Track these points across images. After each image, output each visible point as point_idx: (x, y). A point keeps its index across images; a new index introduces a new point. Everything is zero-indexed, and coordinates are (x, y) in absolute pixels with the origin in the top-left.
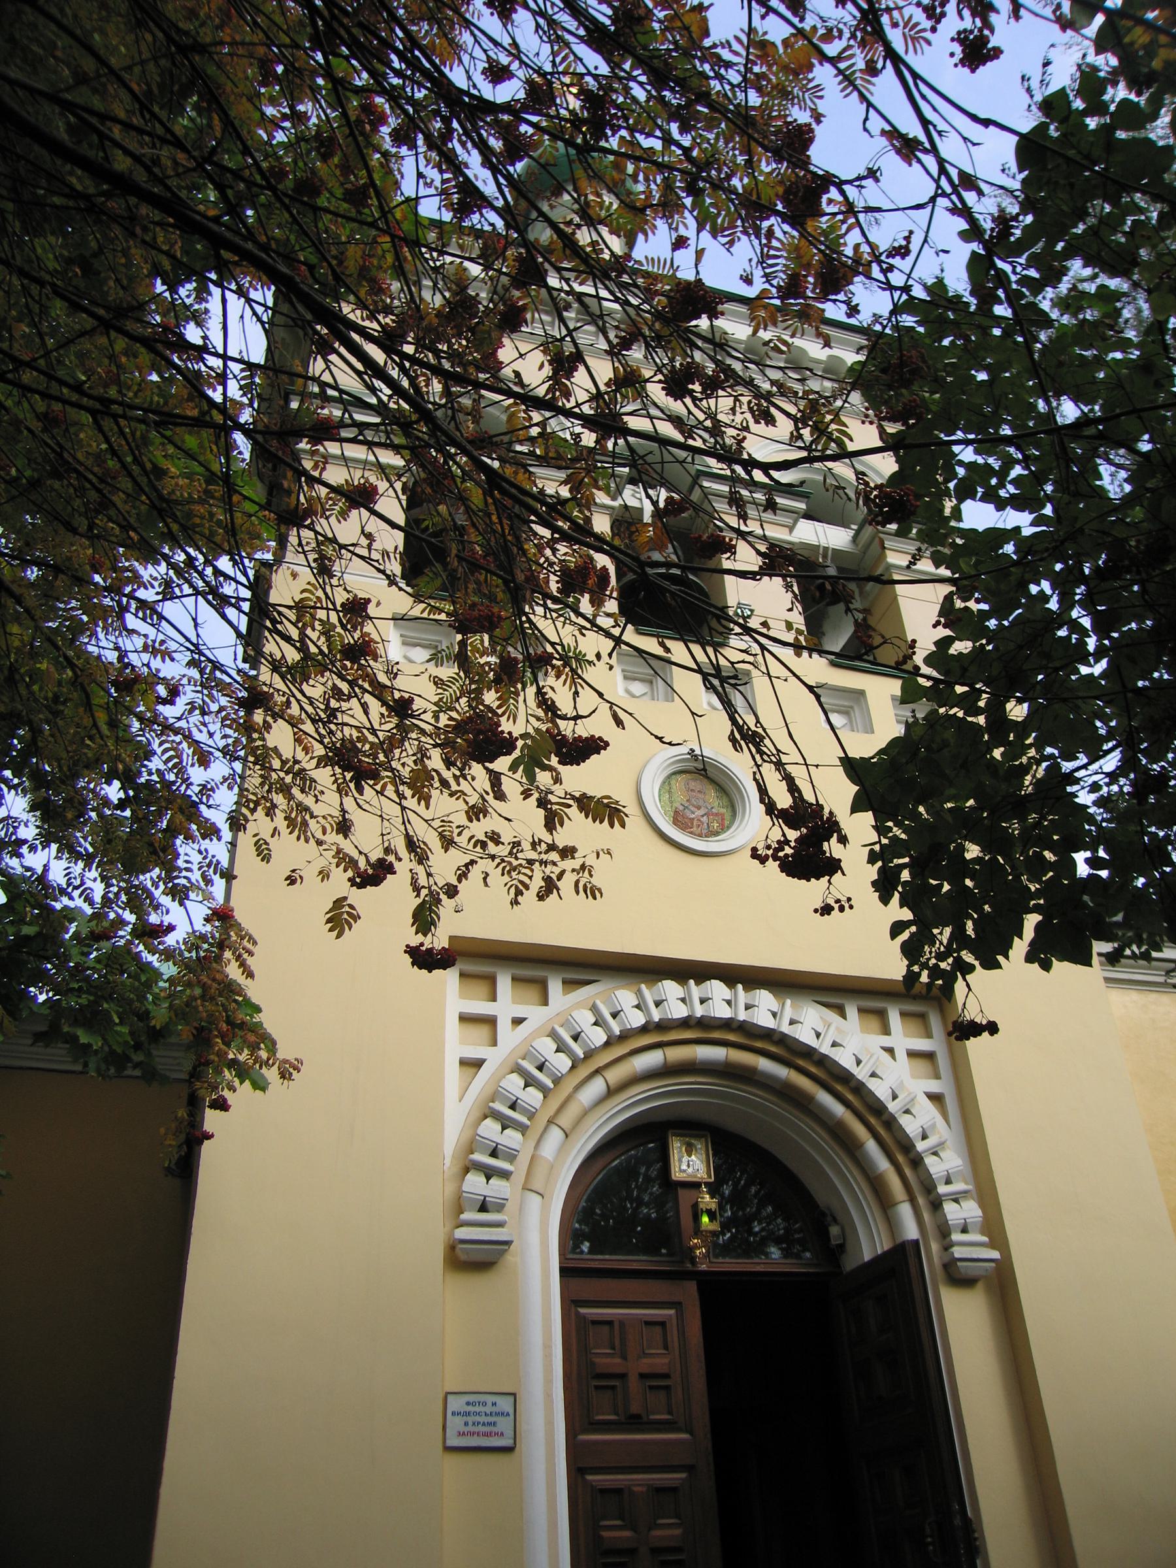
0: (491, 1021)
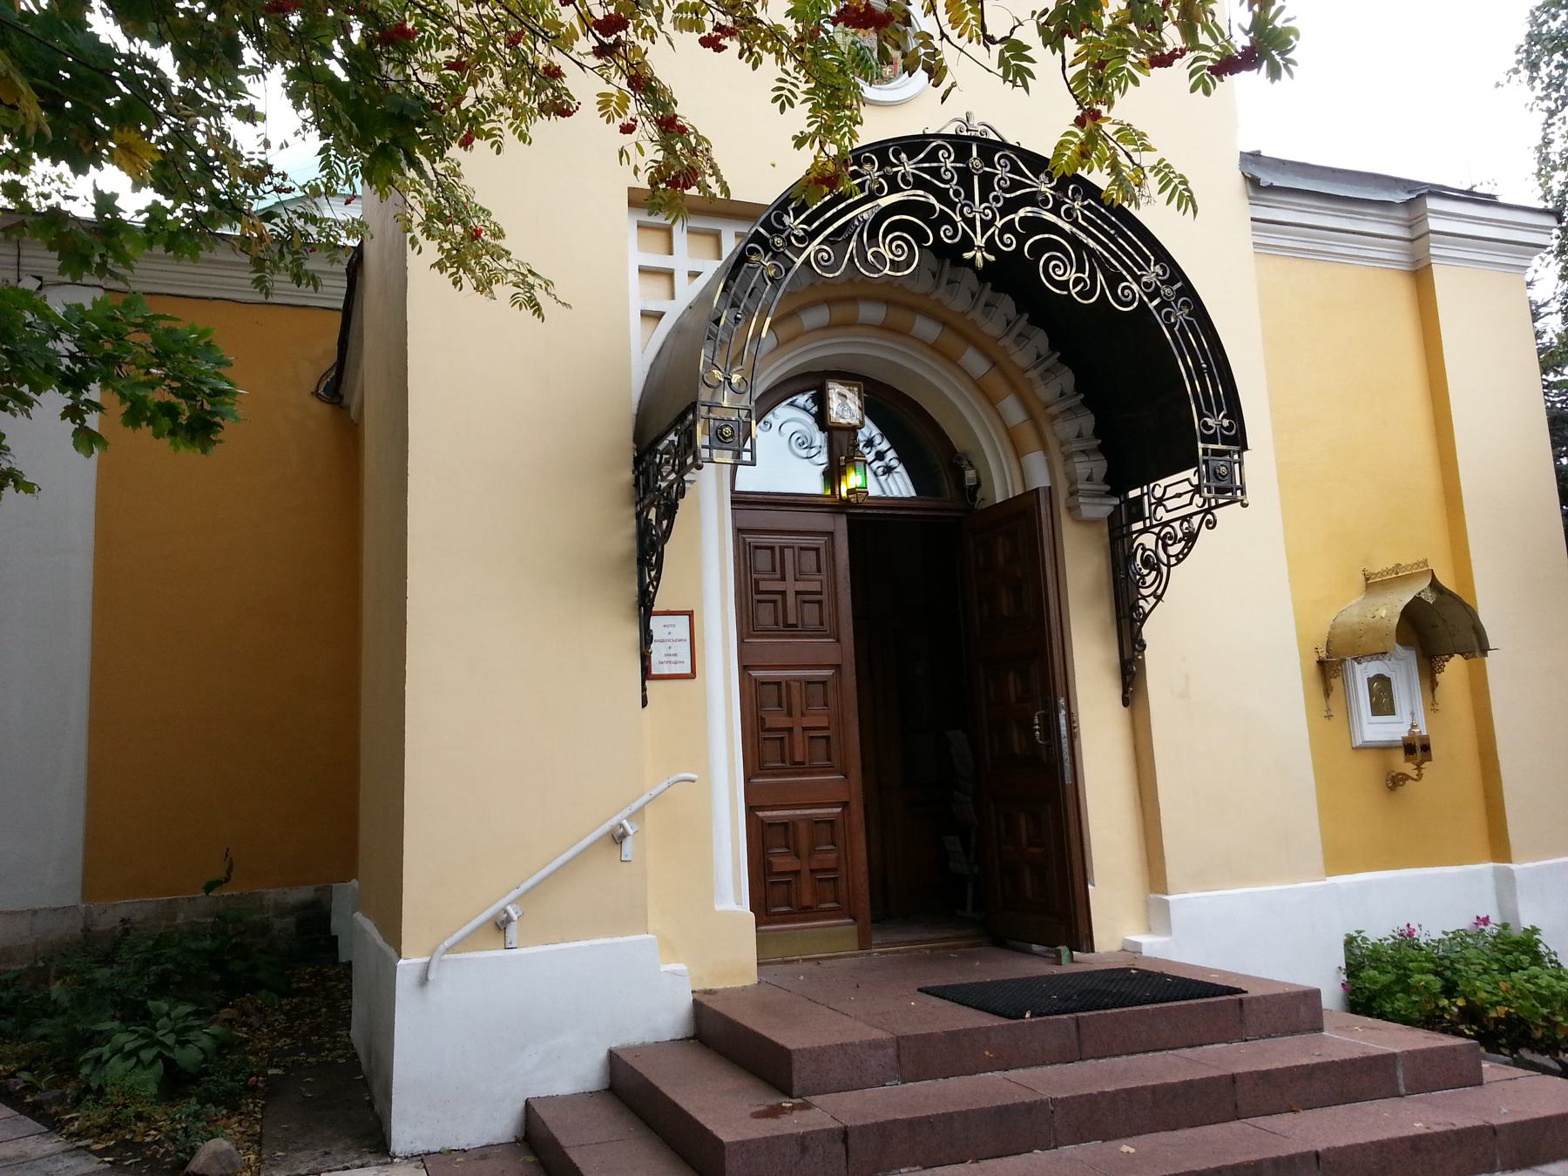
0: (669, 274)
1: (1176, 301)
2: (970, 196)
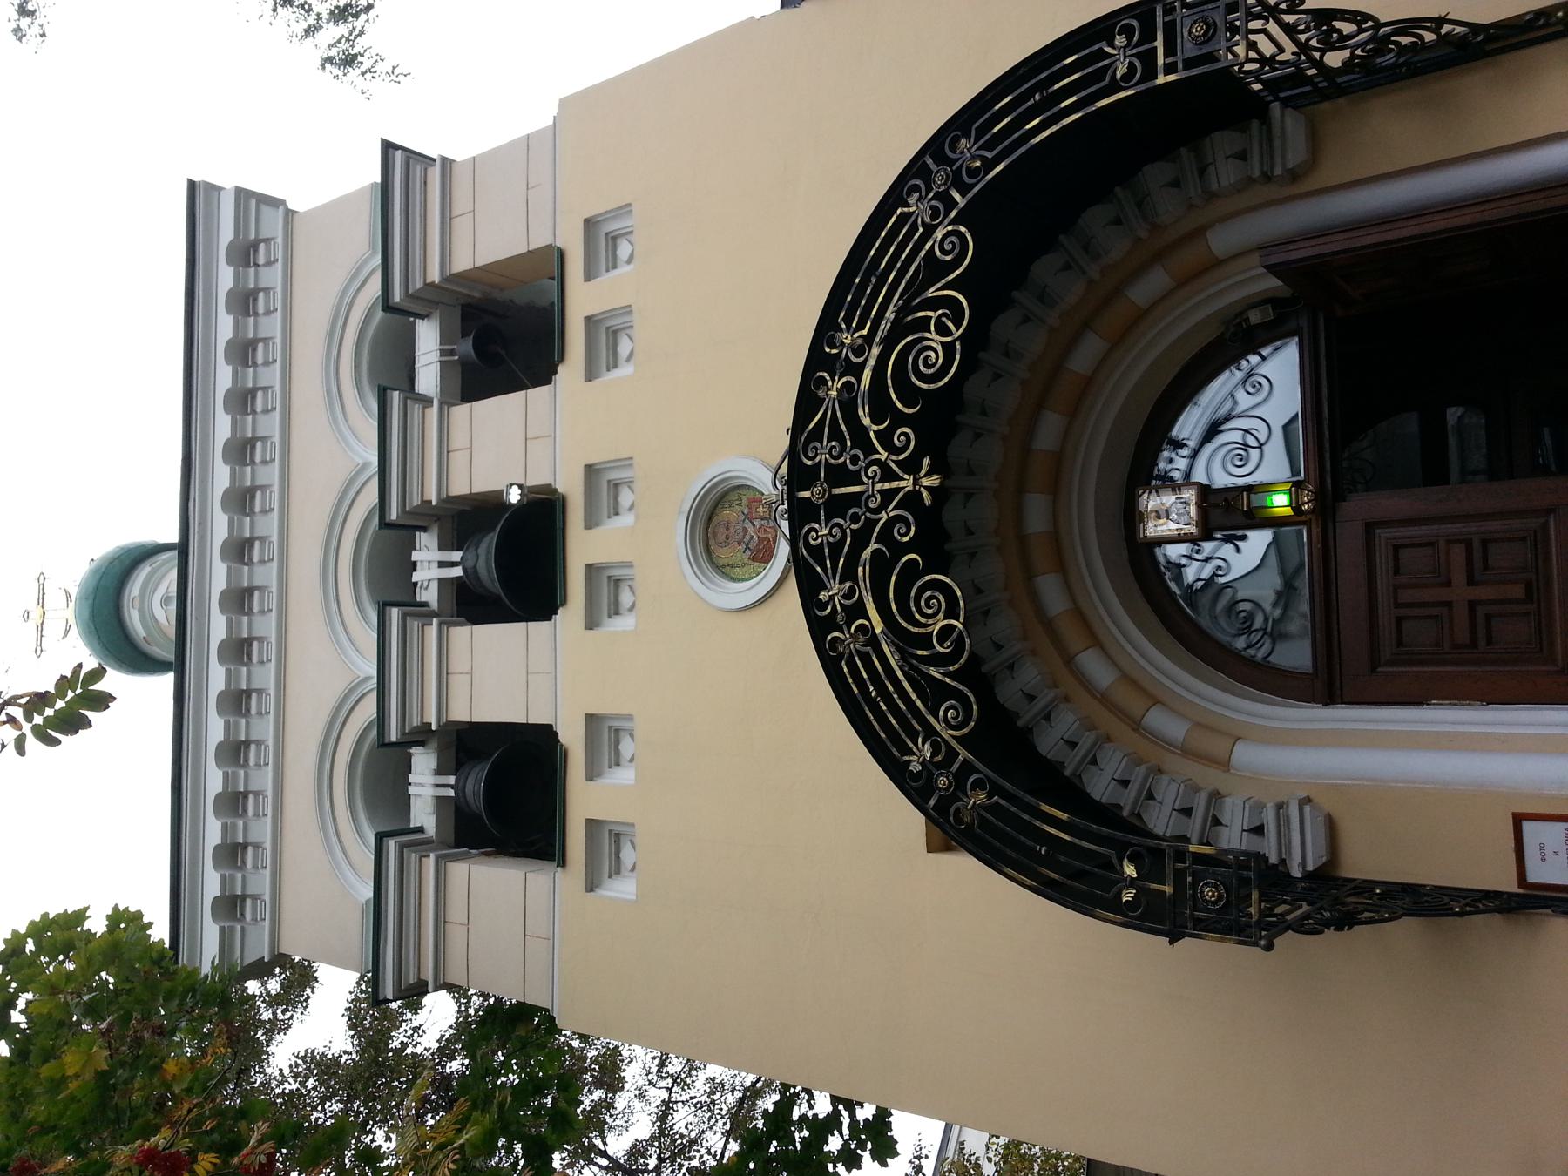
1: (951, 162)
2: (855, 499)
